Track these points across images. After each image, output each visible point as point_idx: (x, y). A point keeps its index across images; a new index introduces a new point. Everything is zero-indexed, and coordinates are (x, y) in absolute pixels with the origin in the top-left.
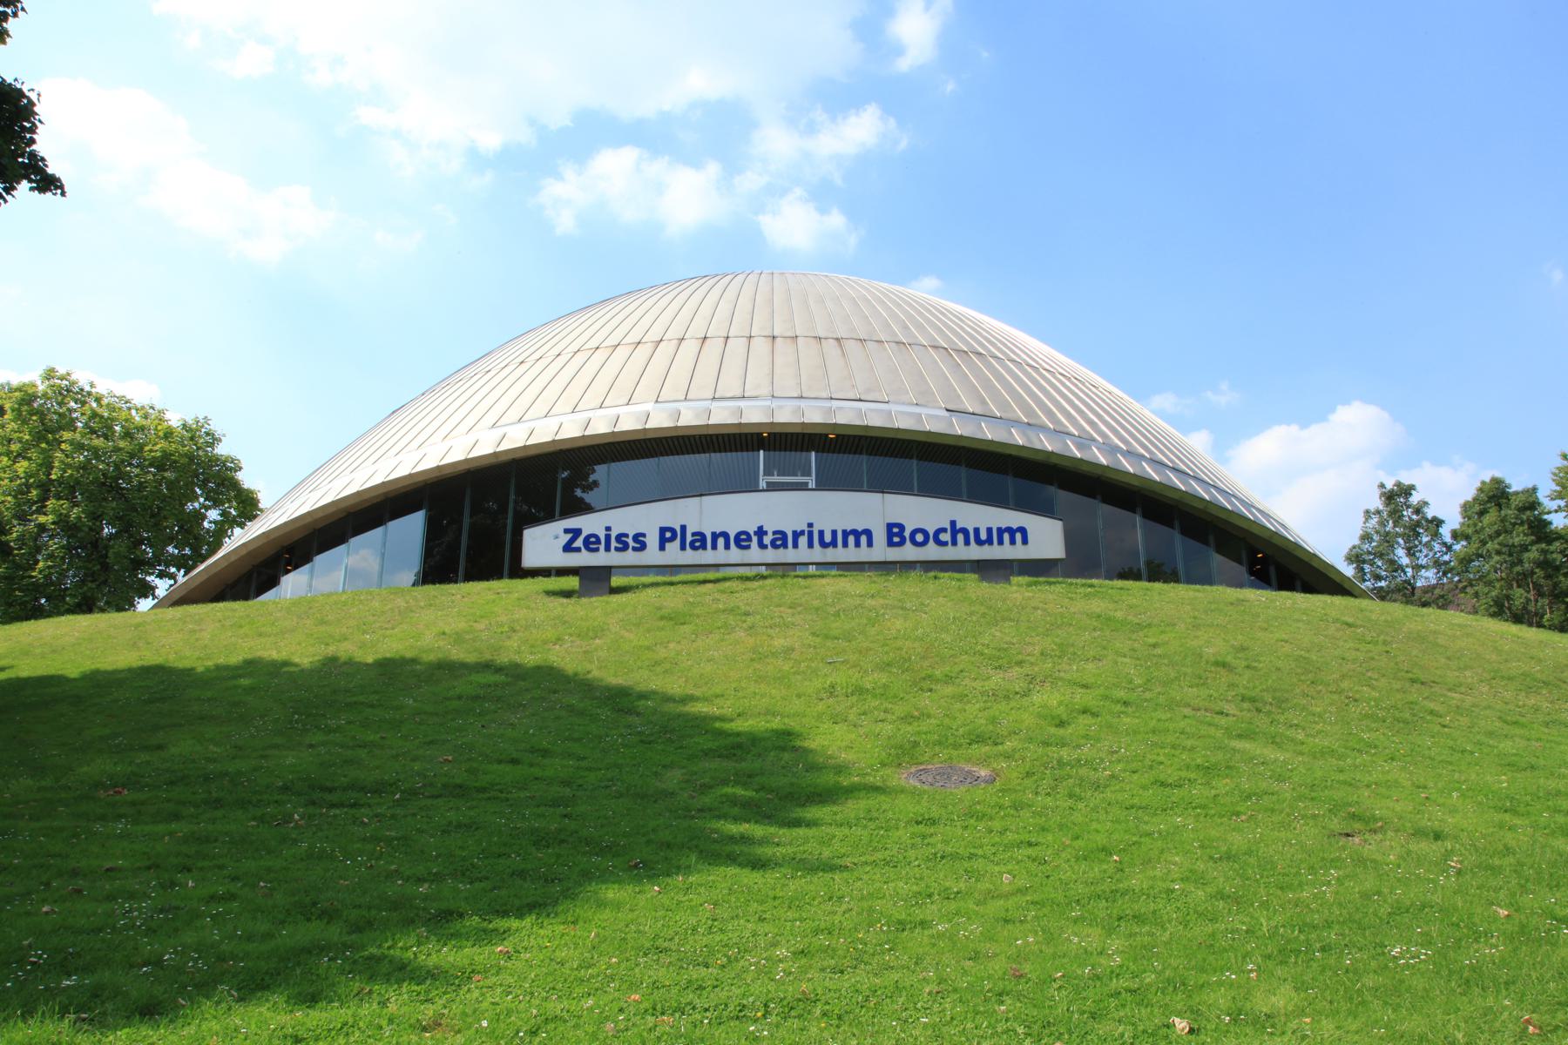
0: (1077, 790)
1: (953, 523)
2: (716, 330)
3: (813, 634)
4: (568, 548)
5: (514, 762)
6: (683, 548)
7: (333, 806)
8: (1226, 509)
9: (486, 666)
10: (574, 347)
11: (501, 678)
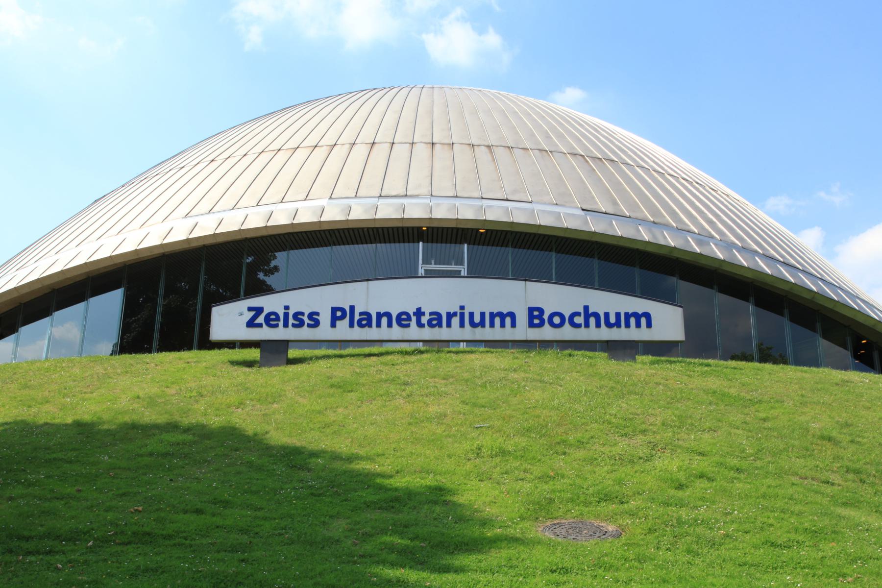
0: (695, 547)
1: (586, 308)
2: (384, 136)
3: (463, 402)
4: (251, 324)
5: (199, 512)
6: (351, 325)
7: (29, 553)
8: (833, 300)
9: (172, 427)
10: (259, 149)
11: (189, 437)
